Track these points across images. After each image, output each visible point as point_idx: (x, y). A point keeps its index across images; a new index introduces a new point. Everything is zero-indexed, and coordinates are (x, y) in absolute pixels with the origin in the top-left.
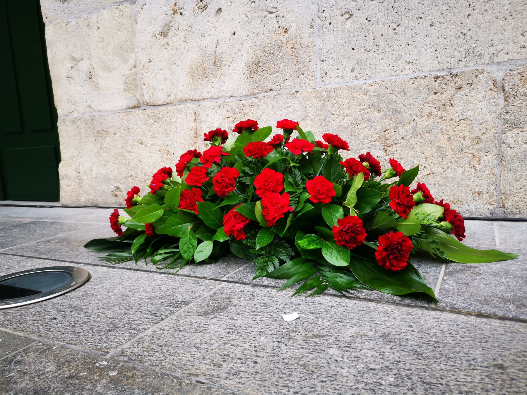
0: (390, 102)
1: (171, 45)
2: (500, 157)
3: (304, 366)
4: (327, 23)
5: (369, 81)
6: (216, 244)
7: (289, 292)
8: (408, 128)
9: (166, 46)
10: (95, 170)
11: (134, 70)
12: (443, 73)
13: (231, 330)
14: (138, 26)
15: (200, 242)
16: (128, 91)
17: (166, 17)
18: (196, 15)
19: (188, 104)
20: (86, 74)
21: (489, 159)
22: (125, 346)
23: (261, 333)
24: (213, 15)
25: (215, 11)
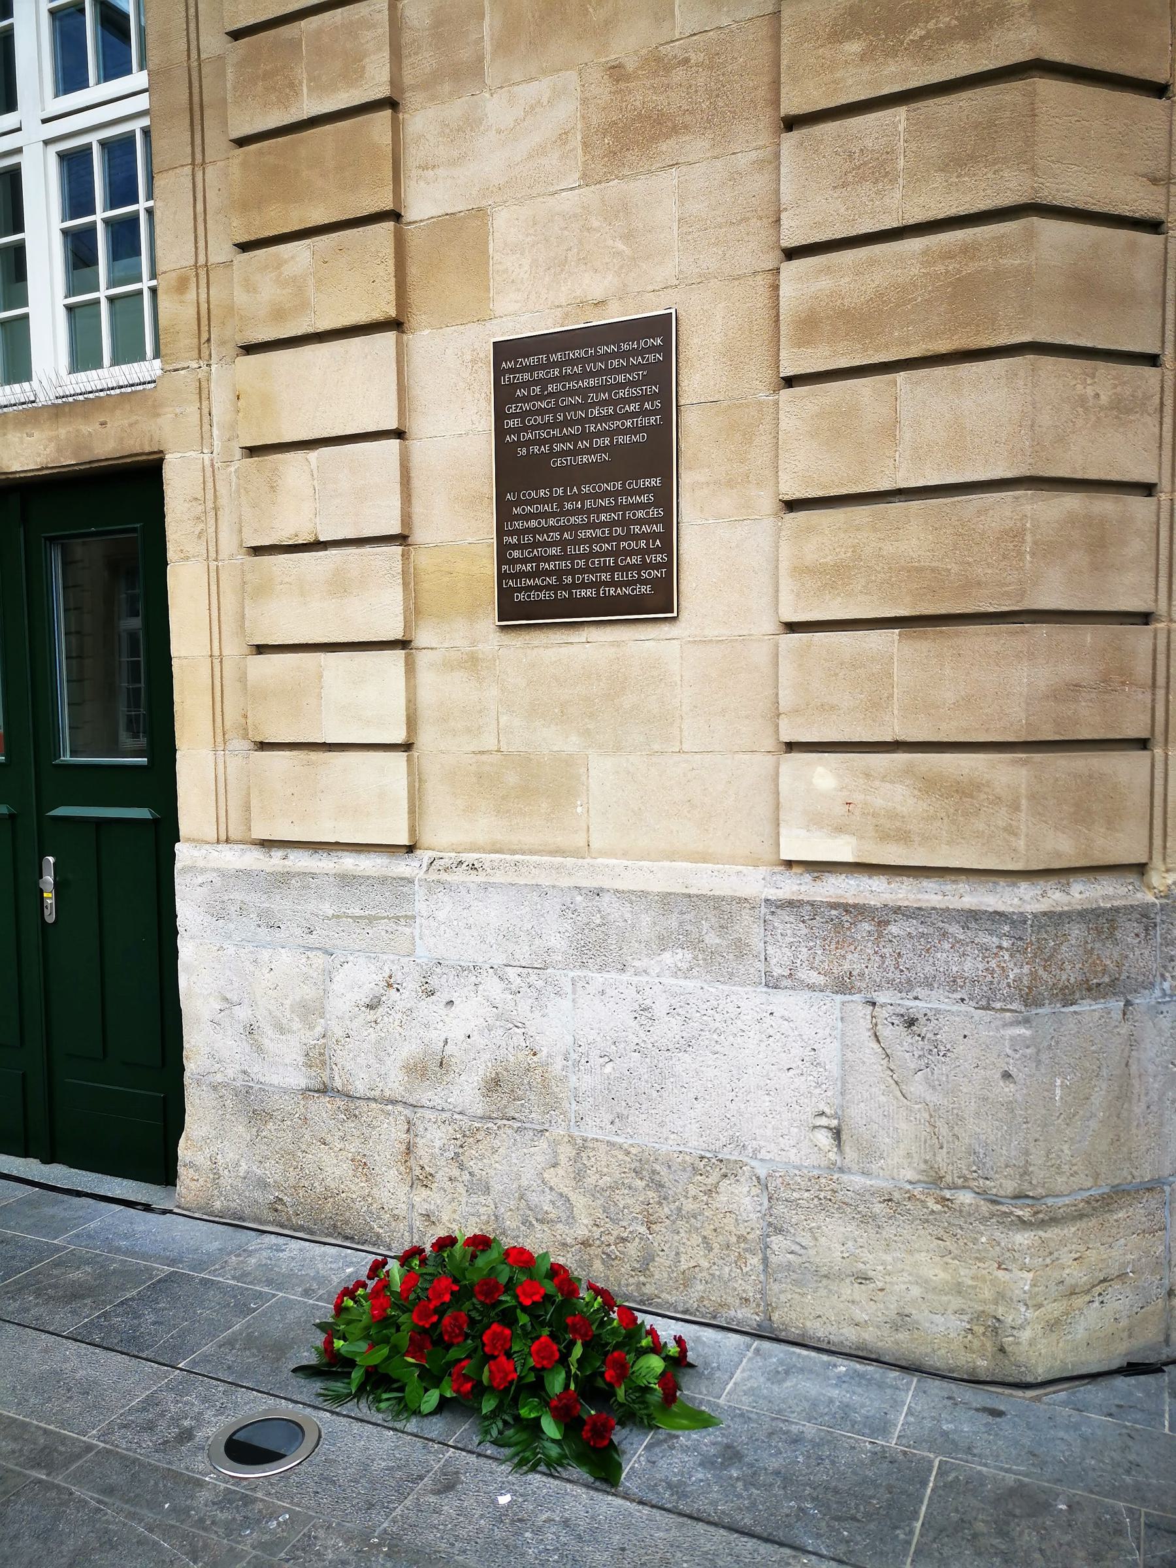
0: (654, 1172)
1: (381, 1025)
2: (765, 1261)
3: (507, 1546)
4: (583, 1061)
5: (630, 1142)
6: (442, 1397)
7: (506, 1468)
8: (673, 1207)
9: (373, 1024)
10: (244, 1167)
11: (323, 1041)
12: (708, 1155)
13: (461, 1511)
14: (334, 986)
15: (426, 1390)
16: (310, 1066)
17: (376, 988)
18: (420, 999)
19: (400, 1108)
20: (245, 1027)
21: (755, 1260)
22: (385, 1525)
23: (482, 1517)
24: (442, 1005)
25: (445, 1001)
